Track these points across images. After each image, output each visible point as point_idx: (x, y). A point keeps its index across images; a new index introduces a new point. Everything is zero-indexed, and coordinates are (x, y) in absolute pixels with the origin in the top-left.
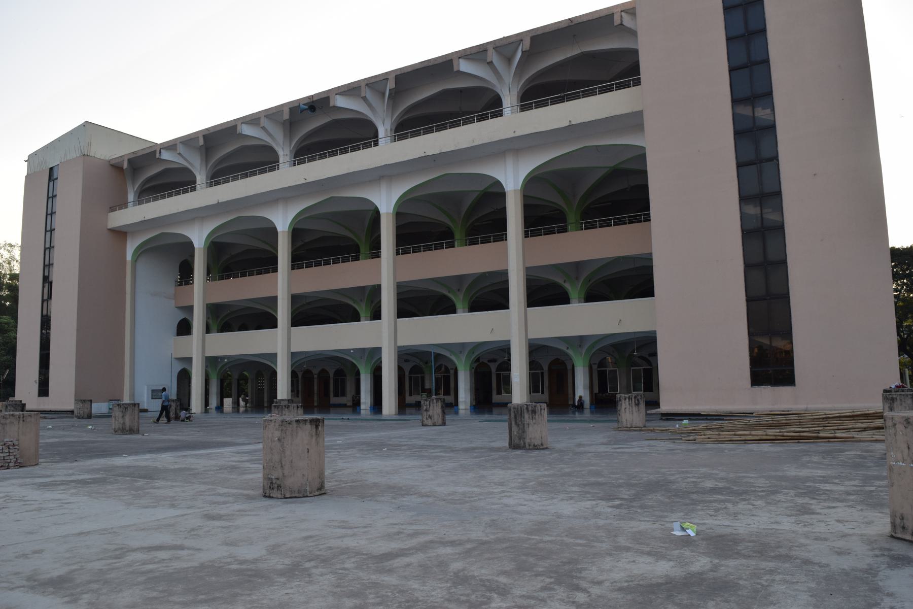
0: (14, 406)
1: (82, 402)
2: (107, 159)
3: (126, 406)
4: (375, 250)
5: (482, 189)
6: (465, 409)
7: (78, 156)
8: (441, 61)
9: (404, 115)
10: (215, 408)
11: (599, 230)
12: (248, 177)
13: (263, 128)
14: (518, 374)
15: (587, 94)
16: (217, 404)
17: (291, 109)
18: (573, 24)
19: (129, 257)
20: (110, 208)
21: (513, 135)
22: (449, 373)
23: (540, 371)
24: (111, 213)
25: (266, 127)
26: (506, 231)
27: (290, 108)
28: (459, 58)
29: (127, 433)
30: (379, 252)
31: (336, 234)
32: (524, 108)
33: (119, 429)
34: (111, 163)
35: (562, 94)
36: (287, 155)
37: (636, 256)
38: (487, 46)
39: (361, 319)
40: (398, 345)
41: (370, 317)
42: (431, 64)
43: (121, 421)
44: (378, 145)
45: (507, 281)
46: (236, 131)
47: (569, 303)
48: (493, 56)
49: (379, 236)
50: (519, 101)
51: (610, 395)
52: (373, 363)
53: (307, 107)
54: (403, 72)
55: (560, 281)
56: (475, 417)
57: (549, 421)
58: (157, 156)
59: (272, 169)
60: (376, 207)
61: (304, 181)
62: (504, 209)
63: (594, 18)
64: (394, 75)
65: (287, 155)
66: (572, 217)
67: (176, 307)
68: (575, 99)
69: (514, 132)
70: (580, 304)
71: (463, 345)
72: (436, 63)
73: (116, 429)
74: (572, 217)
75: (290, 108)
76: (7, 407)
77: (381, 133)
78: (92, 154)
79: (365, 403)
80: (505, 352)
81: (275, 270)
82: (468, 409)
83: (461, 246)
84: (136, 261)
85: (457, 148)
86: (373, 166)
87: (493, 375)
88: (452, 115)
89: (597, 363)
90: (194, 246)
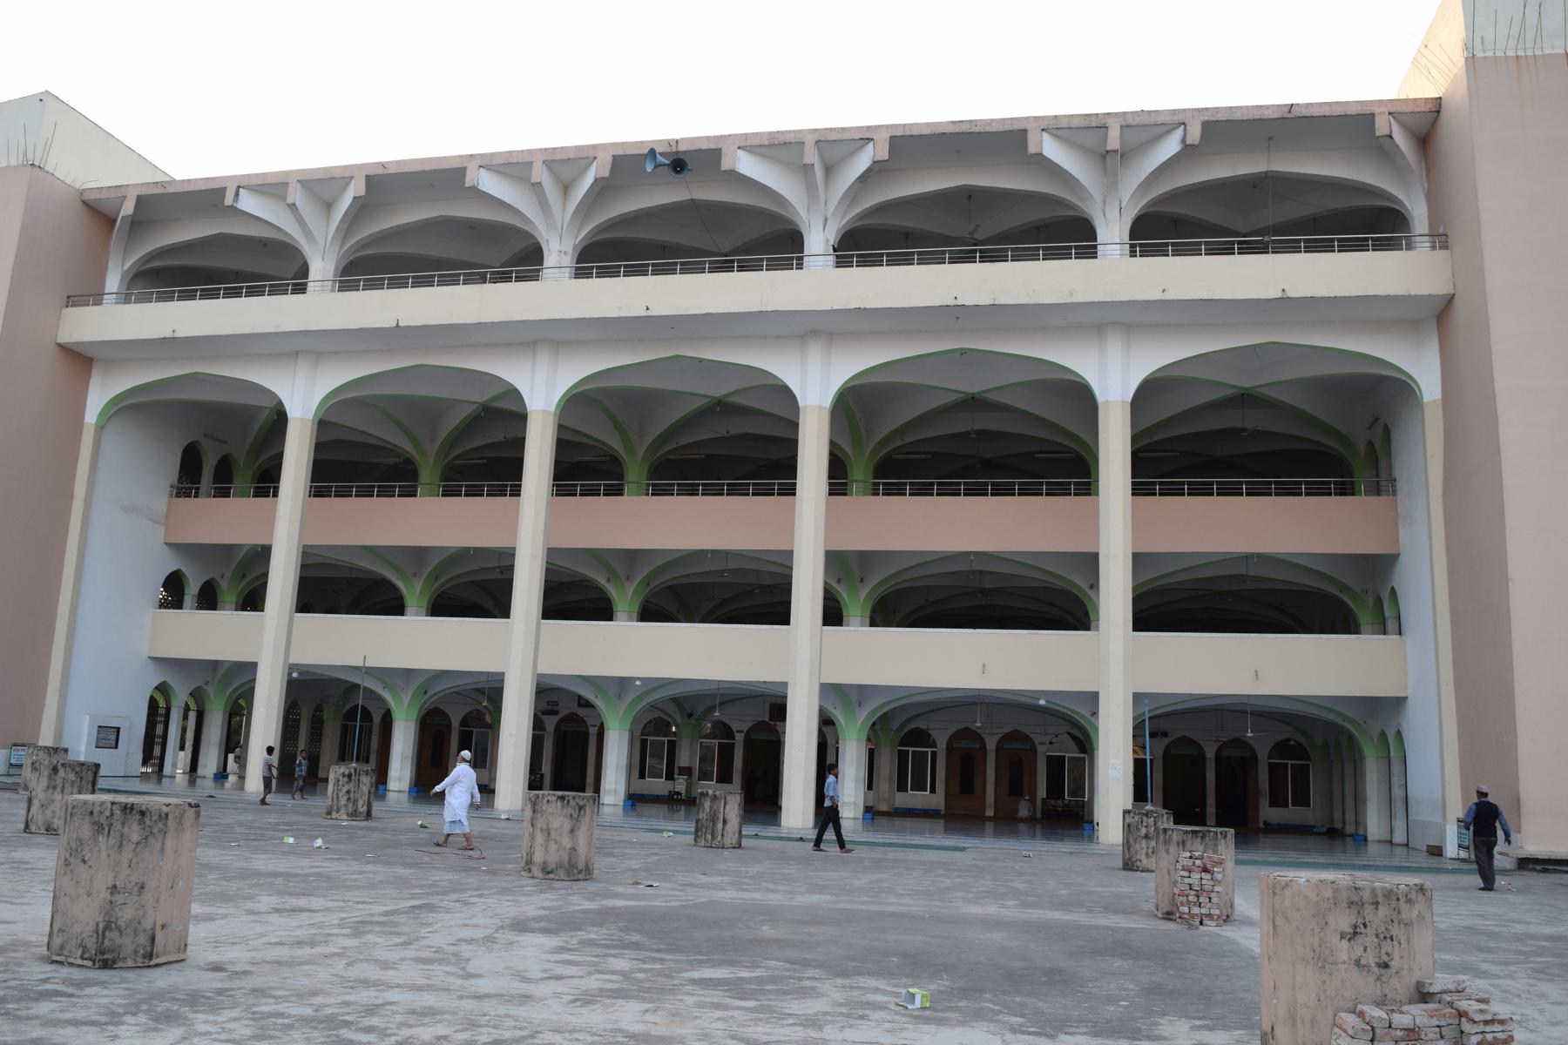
0: (78, 769)
1: (49, 754)
2: (77, 186)
3: (581, 803)
4: (267, 482)
5: (482, 400)
6: (854, 819)
7: (14, 163)
8: (1000, 128)
9: (596, 234)
10: (212, 776)
11: (1244, 499)
12: (485, 282)
13: (293, 206)
14: (1119, 761)
15: (925, 260)
16: (217, 769)
17: (616, 159)
18: (1292, 115)
19: (91, 415)
20: (68, 297)
21: (1159, 296)
22: (734, 739)
23: (929, 750)
24: (71, 310)
25: (298, 207)
26: (521, 481)
27: (614, 156)
28: (1043, 130)
29: (580, 876)
30: (1089, 483)
31: (380, 439)
32: (581, 273)
33: (559, 866)
34: (86, 197)
35: (1266, 239)
36: (565, 253)
37: (1282, 557)
38: (1108, 121)
39: (1363, 628)
40: (290, 662)
41: (237, 604)
42: (977, 130)
43: (566, 842)
44: (305, 293)
45: (511, 568)
46: (464, 183)
47: (610, 618)
48: (296, 195)
49: (280, 455)
50: (575, 261)
51: (1072, 803)
52: (228, 694)
53: (667, 162)
54: (908, 133)
55: (600, 579)
56: (634, 821)
57: (1238, 862)
58: (229, 200)
59: (785, 265)
60: (280, 403)
61: (643, 313)
62: (520, 442)
63: (1335, 114)
64: (889, 135)
65: (565, 253)
66: (635, 472)
67: (166, 543)
68: (603, 277)
69: (1164, 291)
70: (237, 612)
71: (408, 673)
72: (988, 129)
73: (551, 866)
74: (427, 474)
75: (614, 156)
76: (55, 770)
77: (550, 259)
78: (49, 168)
79: (615, 792)
80: (484, 694)
81: (790, 491)
82: (857, 819)
83: (864, 495)
84: (103, 427)
85: (1032, 301)
86: (827, 307)
87: (453, 733)
88: (238, 276)
89: (746, 729)
90: (798, 403)
